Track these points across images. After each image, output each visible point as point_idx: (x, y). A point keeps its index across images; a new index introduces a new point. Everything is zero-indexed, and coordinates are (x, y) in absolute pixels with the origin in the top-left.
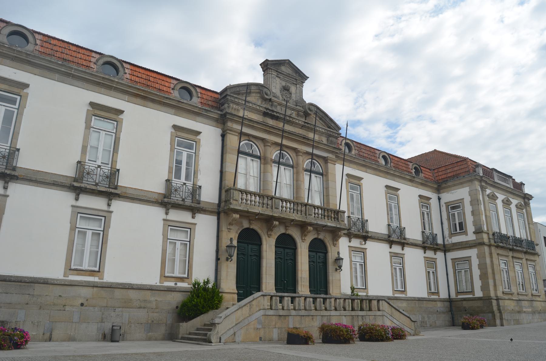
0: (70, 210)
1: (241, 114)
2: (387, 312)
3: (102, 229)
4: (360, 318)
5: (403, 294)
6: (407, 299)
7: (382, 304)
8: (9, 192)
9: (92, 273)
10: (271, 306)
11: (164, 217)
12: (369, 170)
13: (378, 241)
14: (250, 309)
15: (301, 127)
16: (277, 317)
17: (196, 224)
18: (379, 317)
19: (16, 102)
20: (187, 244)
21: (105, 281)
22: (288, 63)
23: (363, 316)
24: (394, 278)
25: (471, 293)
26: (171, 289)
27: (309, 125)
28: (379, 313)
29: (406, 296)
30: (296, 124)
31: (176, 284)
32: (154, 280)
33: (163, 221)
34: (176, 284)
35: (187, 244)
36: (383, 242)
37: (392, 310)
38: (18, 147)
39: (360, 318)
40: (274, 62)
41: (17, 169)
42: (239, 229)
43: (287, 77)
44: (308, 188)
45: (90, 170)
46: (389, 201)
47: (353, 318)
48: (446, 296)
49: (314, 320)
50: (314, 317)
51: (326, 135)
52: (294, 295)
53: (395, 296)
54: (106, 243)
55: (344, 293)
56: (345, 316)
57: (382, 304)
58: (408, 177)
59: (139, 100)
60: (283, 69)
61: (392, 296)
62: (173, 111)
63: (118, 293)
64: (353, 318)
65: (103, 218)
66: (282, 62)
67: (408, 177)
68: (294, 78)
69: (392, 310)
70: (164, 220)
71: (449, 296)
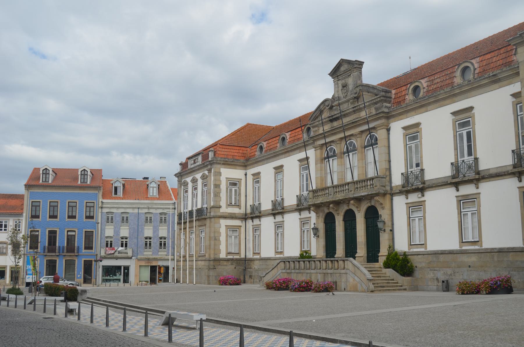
0: (405, 206)
1: (321, 131)
2: (351, 270)
3: (238, 235)
4: (329, 275)
5: (281, 254)
6: (477, 252)
7: (347, 264)
8: (285, 219)
9: (474, 243)
10: (285, 267)
11: (299, 217)
12: (429, 108)
13: (437, 188)
14: (277, 269)
15: (354, 113)
16: (287, 274)
17: (480, 193)
18: (343, 274)
19: (414, 140)
20: (463, 214)
21: (428, 250)
22: (342, 61)
23: (331, 273)
24: (259, 243)
25: (238, 254)
26: (517, 249)
27: (356, 108)
28: (343, 271)
29: (426, 250)
30: (350, 113)
31: (233, 257)
32: (455, 245)
33: (456, 198)
34: (233, 257)
35: (463, 214)
36: (446, 187)
37: (355, 269)
38: (424, 169)
39: (329, 275)
40: (333, 71)
41: (480, 173)
42: (323, 215)
43: (345, 74)
44: (330, 172)
45: (468, 167)
46: (237, 189)
47: (325, 275)
48: (244, 257)
49: (303, 275)
50: (303, 274)
51: (372, 105)
52: (332, 259)
53: (462, 249)
54: (459, 222)
55: (401, 250)
56: (320, 273)
57: (347, 264)
58: (486, 81)
59: (256, 165)
60: (342, 69)
61: (459, 249)
62: (298, 151)
63: (442, 258)
64: (325, 275)
65: (238, 229)
66: (338, 65)
67: (486, 81)
68: (348, 71)
69: (355, 269)
70: (300, 219)
71: (246, 256)
